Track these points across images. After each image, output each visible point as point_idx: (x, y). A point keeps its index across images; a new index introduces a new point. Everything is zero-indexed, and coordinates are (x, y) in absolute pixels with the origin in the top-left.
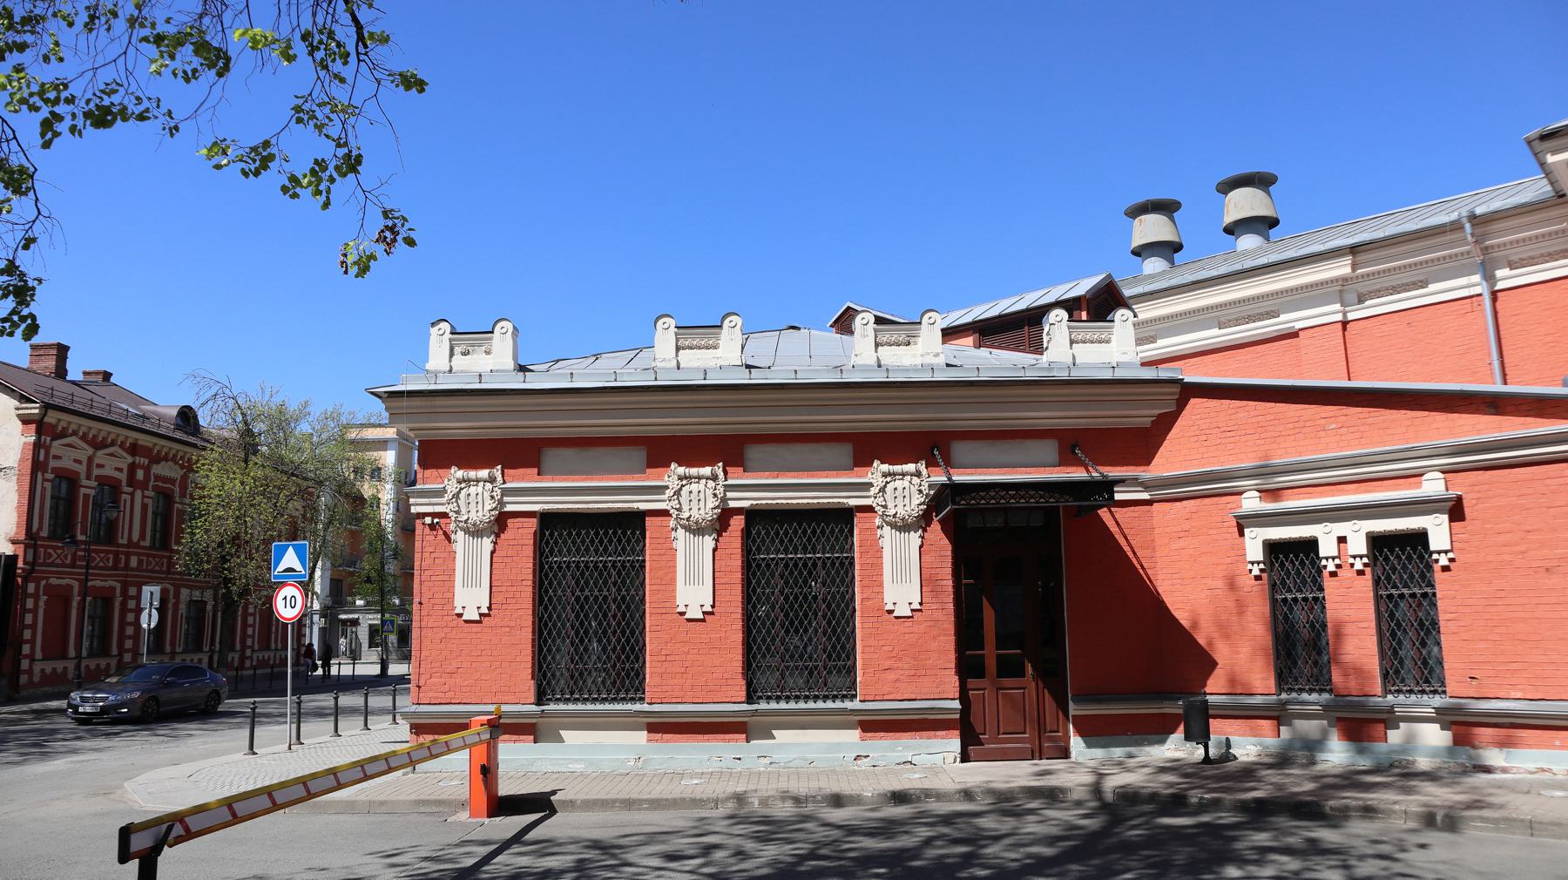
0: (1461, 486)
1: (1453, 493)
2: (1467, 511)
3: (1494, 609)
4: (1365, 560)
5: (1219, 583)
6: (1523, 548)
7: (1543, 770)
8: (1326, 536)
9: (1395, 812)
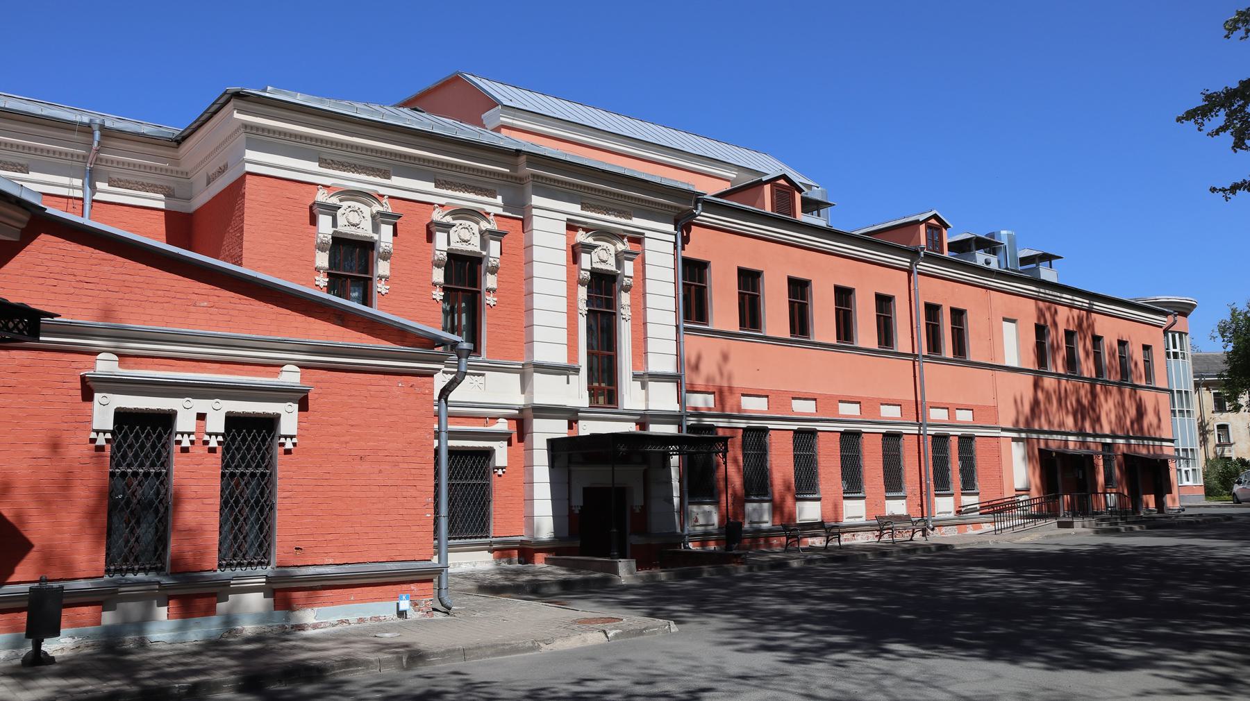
0: (318, 383)
1: (304, 386)
2: (310, 403)
3: (321, 489)
4: (109, 436)
5: (42, 451)
6: (347, 438)
7: (342, 622)
8: (185, 412)
9: (371, 662)
